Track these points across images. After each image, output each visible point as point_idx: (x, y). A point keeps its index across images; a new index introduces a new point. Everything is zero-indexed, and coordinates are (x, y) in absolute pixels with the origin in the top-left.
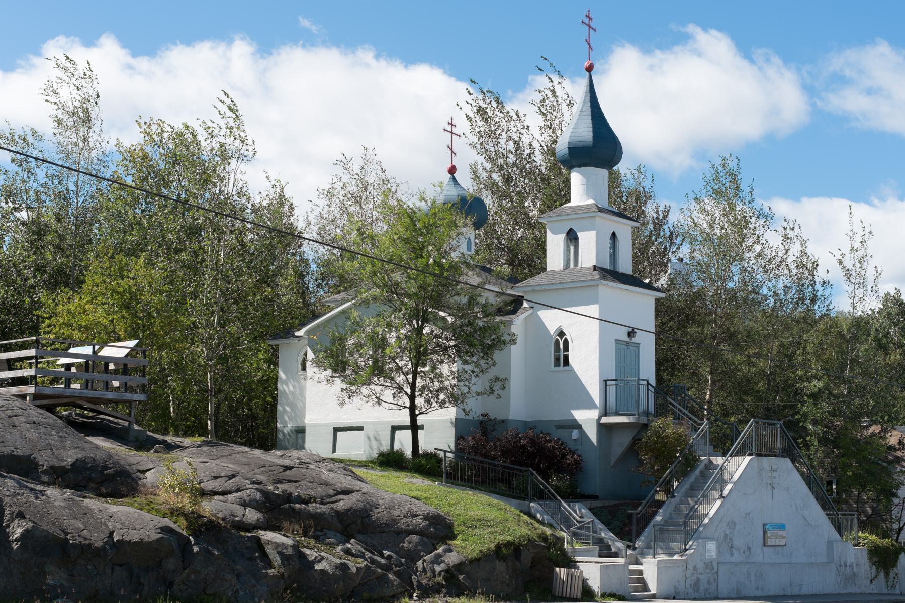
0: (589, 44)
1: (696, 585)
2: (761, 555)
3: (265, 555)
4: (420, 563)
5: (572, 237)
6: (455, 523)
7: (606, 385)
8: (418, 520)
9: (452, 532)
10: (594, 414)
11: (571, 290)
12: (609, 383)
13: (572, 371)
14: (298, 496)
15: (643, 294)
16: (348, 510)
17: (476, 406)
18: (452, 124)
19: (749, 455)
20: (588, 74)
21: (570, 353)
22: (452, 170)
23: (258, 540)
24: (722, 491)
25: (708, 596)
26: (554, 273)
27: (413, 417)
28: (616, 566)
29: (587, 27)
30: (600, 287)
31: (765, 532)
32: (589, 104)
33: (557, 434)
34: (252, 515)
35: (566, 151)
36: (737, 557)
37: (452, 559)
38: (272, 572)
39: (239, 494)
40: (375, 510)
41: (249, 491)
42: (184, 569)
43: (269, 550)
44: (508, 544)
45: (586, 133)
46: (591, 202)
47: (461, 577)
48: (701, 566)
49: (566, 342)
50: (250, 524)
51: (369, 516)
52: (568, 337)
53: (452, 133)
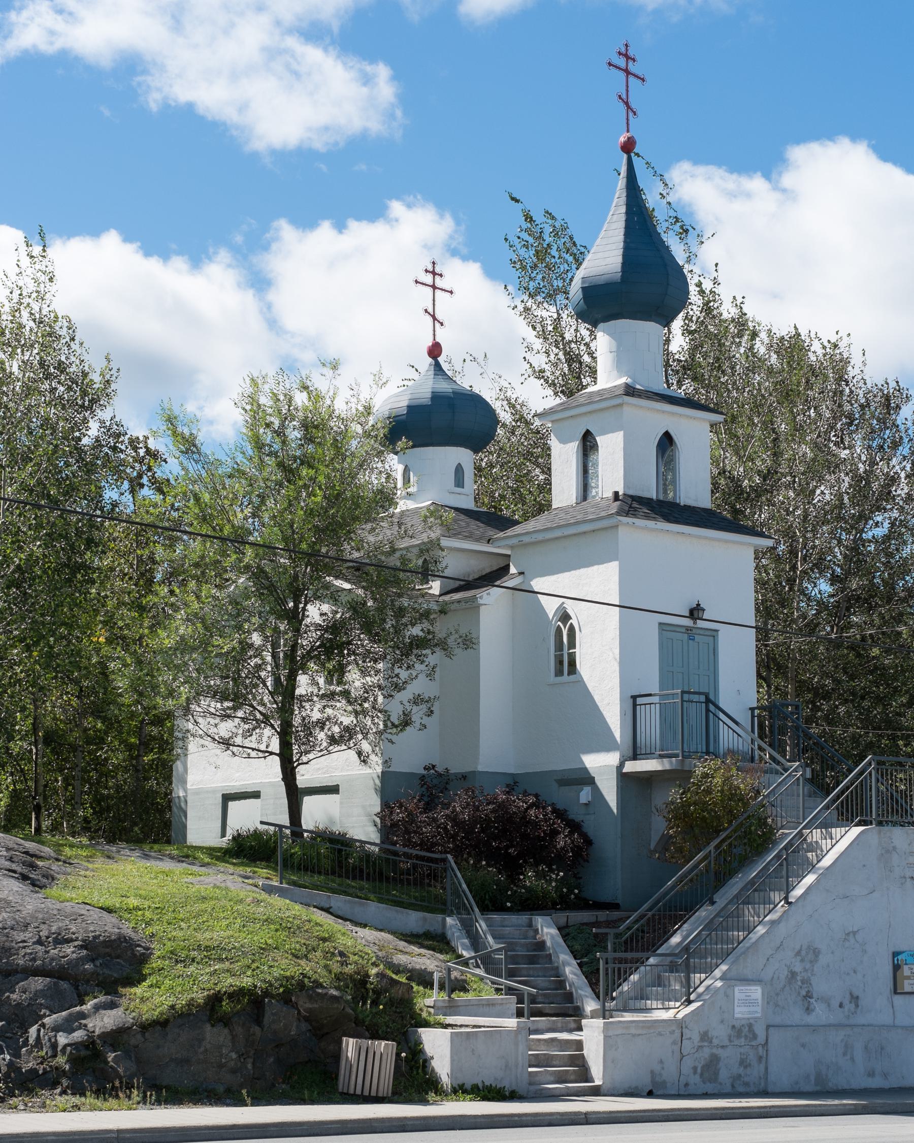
0: (627, 103)
1: (711, 1067)
2: (879, 1007)
7: (635, 705)
10: (612, 759)
11: (582, 540)
12: (640, 701)
13: (581, 682)
15: (727, 541)
17: (415, 752)
18: (434, 273)
19: (858, 824)
20: (625, 156)
21: (577, 650)
22: (435, 351)
24: (788, 893)
25: (741, 1089)
28: (495, 1034)
29: (622, 75)
30: (621, 530)
31: (896, 968)
36: (820, 1014)
44: (237, 994)
47: (111, 1056)
48: (720, 1033)
49: (572, 630)
52: (574, 621)
53: (434, 287)
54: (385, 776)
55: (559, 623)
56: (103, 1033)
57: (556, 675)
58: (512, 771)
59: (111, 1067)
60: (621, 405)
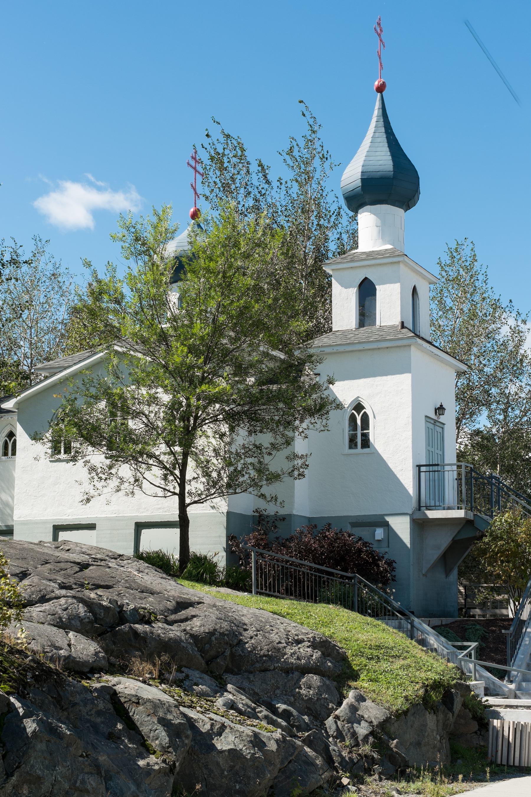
0: (195, 189)
3: (131, 725)
4: (330, 722)
5: (367, 291)
6: (349, 653)
7: (420, 472)
8: (304, 650)
9: (350, 666)
11: (376, 352)
14: (135, 610)
16: (212, 633)
23: (112, 695)
26: (344, 333)
27: (183, 507)
30: (413, 348)
32: (383, 130)
33: (359, 532)
34: (85, 648)
35: (359, 183)
37: (372, 712)
38: (153, 761)
39: (46, 606)
40: (245, 634)
41: (63, 601)
42: (9, 775)
43: (138, 714)
45: (384, 162)
46: (389, 247)
49: (365, 419)
50: (85, 663)
51: (241, 643)
54: (229, 514)
55: (353, 411)
56: (380, 722)
57: (350, 447)
58: (308, 516)
59: (396, 752)
60: (399, 262)
